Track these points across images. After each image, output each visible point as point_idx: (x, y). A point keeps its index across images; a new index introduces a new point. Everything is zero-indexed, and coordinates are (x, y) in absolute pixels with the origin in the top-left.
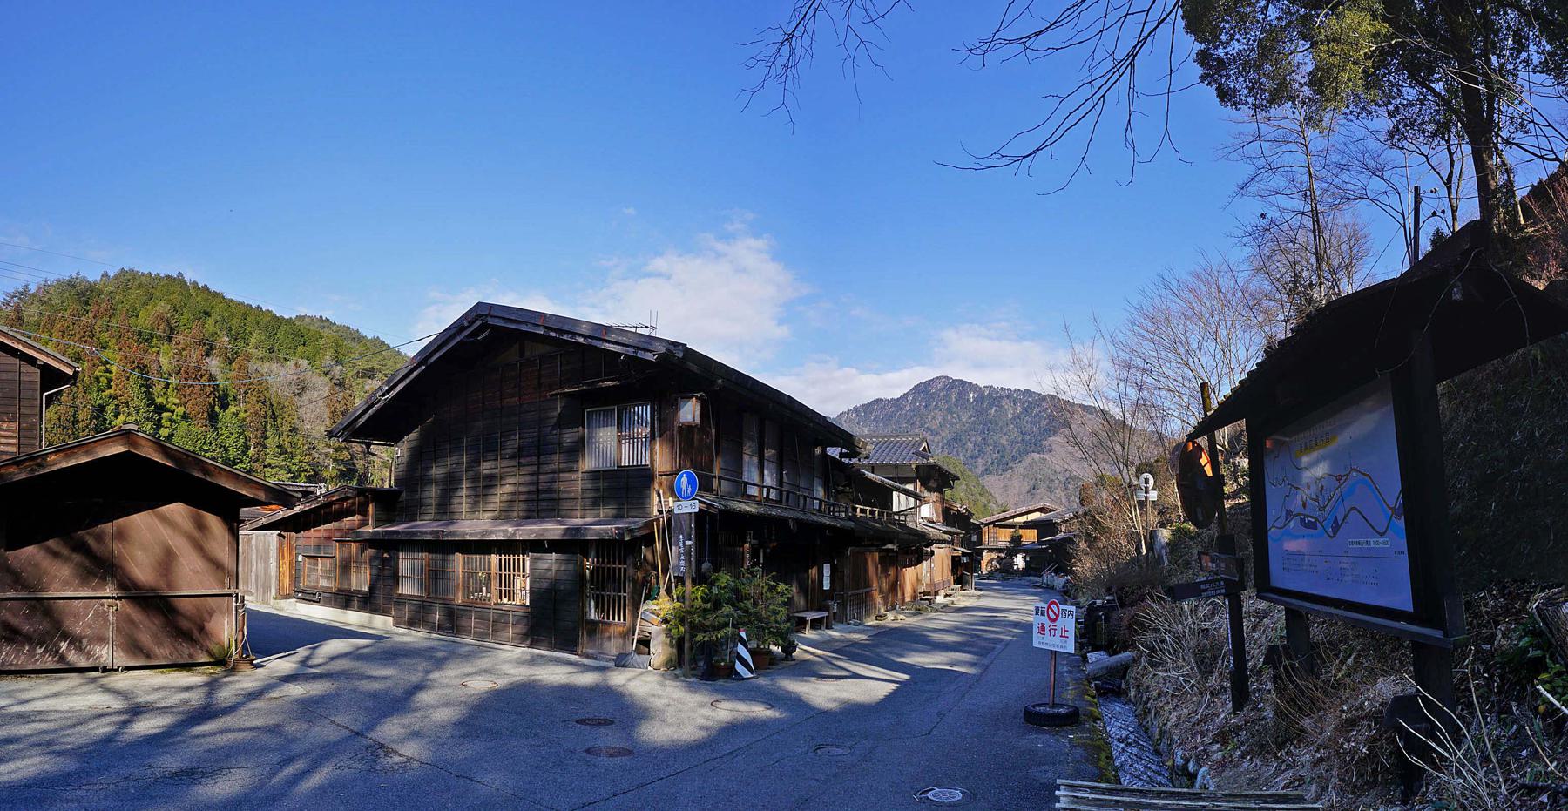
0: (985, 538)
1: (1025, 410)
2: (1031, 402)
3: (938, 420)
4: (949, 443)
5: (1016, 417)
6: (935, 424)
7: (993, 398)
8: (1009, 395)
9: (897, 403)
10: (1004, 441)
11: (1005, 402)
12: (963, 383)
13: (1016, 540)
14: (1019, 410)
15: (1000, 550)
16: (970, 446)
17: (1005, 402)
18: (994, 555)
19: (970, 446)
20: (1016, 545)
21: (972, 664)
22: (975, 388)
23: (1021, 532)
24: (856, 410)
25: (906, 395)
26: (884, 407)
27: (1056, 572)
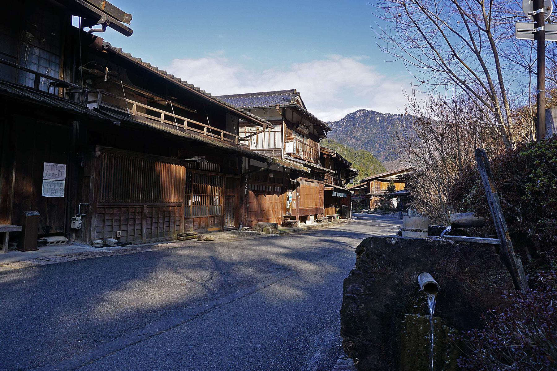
0: (372, 188)
4: (365, 144)
12: (373, 112)
13: (391, 189)
15: (381, 196)
16: (377, 145)
18: (378, 199)
19: (377, 145)
22: (380, 115)
23: (395, 184)
25: (343, 119)
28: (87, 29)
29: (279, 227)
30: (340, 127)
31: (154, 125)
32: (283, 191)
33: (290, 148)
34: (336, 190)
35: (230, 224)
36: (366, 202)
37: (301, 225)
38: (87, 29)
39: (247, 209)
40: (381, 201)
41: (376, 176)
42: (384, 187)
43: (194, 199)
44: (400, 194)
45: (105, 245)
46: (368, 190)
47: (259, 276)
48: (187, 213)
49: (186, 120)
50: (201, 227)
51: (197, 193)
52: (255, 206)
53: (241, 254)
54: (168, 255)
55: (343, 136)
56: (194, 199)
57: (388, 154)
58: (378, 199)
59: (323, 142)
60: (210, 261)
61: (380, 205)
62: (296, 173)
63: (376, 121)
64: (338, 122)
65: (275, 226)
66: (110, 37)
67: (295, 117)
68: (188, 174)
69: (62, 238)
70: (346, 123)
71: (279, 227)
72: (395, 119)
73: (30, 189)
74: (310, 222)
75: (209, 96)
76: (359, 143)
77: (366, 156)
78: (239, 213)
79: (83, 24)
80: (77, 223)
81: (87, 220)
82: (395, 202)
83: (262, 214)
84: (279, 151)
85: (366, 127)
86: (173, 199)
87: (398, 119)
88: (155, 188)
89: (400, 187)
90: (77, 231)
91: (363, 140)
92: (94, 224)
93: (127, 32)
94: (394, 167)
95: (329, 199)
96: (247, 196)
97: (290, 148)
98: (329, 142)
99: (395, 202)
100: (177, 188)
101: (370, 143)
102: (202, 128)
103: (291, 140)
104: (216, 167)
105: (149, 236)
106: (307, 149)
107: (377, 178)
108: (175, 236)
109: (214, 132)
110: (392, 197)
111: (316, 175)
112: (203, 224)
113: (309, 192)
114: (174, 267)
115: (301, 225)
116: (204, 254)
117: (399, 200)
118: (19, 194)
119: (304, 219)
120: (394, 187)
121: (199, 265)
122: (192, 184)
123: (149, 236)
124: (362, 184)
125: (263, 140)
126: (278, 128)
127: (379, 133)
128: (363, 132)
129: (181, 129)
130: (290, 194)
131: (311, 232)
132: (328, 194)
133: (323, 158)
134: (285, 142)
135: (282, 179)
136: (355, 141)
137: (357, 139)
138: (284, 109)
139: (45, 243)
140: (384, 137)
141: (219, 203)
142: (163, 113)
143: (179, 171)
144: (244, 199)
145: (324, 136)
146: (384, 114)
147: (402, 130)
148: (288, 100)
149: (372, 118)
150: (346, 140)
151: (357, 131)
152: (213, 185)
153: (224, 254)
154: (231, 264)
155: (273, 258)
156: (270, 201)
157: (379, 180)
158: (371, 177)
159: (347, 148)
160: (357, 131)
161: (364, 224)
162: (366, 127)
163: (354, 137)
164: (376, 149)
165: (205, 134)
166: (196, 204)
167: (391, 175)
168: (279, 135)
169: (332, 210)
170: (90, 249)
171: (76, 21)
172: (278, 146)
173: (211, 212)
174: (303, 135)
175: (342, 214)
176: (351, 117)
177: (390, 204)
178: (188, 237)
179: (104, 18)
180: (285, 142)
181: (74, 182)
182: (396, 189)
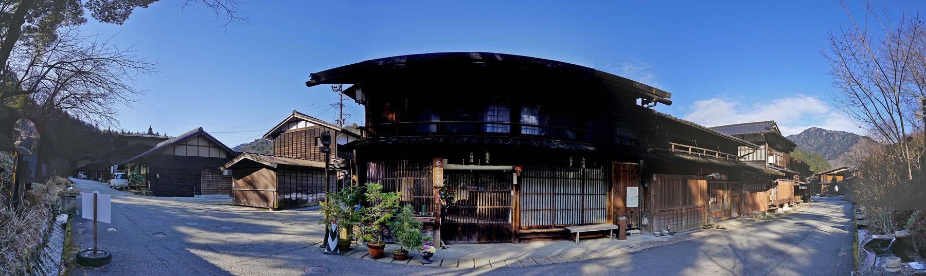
13: (834, 180)
22: (825, 131)
28: (645, 106)
29: (767, 214)
31: (685, 157)
32: (768, 189)
33: (771, 160)
34: (801, 185)
35: (735, 214)
36: (818, 190)
37: (780, 210)
38: (645, 106)
39: (745, 204)
42: (830, 178)
43: (712, 200)
45: (662, 235)
47: (765, 261)
48: (708, 209)
49: (705, 150)
50: (717, 218)
51: (714, 196)
52: (750, 201)
53: (749, 241)
54: (702, 244)
56: (712, 200)
59: (792, 154)
60: (730, 250)
62: (776, 177)
65: (764, 213)
66: (659, 108)
67: (770, 137)
68: (708, 185)
69: (637, 231)
71: (767, 214)
73: (620, 203)
74: (786, 208)
75: (704, 128)
78: (742, 208)
79: (643, 103)
80: (645, 221)
81: (651, 219)
82: (837, 188)
83: (755, 206)
84: (764, 162)
86: (700, 202)
88: (689, 198)
90: (645, 226)
92: (655, 222)
93: (669, 103)
94: (837, 165)
95: (797, 191)
96: (745, 195)
97: (771, 160)
99: (837, 188)
100: (702, 195)
101: (819, 148)
102: (715, 154)
103: (771, 155)
104: (725, 177)
105: (687, 227)
106: (781, 159)
108: (701, 226)
109: (722, 155)
111: (789, 176)
112: (718, 216)
113: (784, 188)
114: (710, 256)
115: (780, 210)
116: (725, 242)
118: (616, 207)
119: (781, 206)
121: (724, 255)
122: (711, 191)
123: (687, 227)
125: (750, 156)
126: (762, 147)
129: (702, 156)
130: (772, 190)
131: (789, 216)
132: (796, 188)
133: (792, 164)
134: (767, 156)
135: (767, 181)
138: (766, 135)
139: (629, 234)
141: (727, 202)
142: (691, 147)
143: (703, 183)
144: (743, 197)
145: (792, 150)
148: (769, 129)
152: (723, 189)
153: (741, 241)
154: (745, 252)
155: (769, 243)
156: (761, 197)
161: (820, 206)
165: (716, 159)
166: (714, 203)
168: (763, 151)
169: (798, 198)
170: (654, 238)
171: (639, 102)
172: (763, 159)
173: (723, 207)
174: (779, 150)
175: (805, 200)
178: (710, 226)
179: (656, 98)
180: (767, 156)
181: (645, 195)
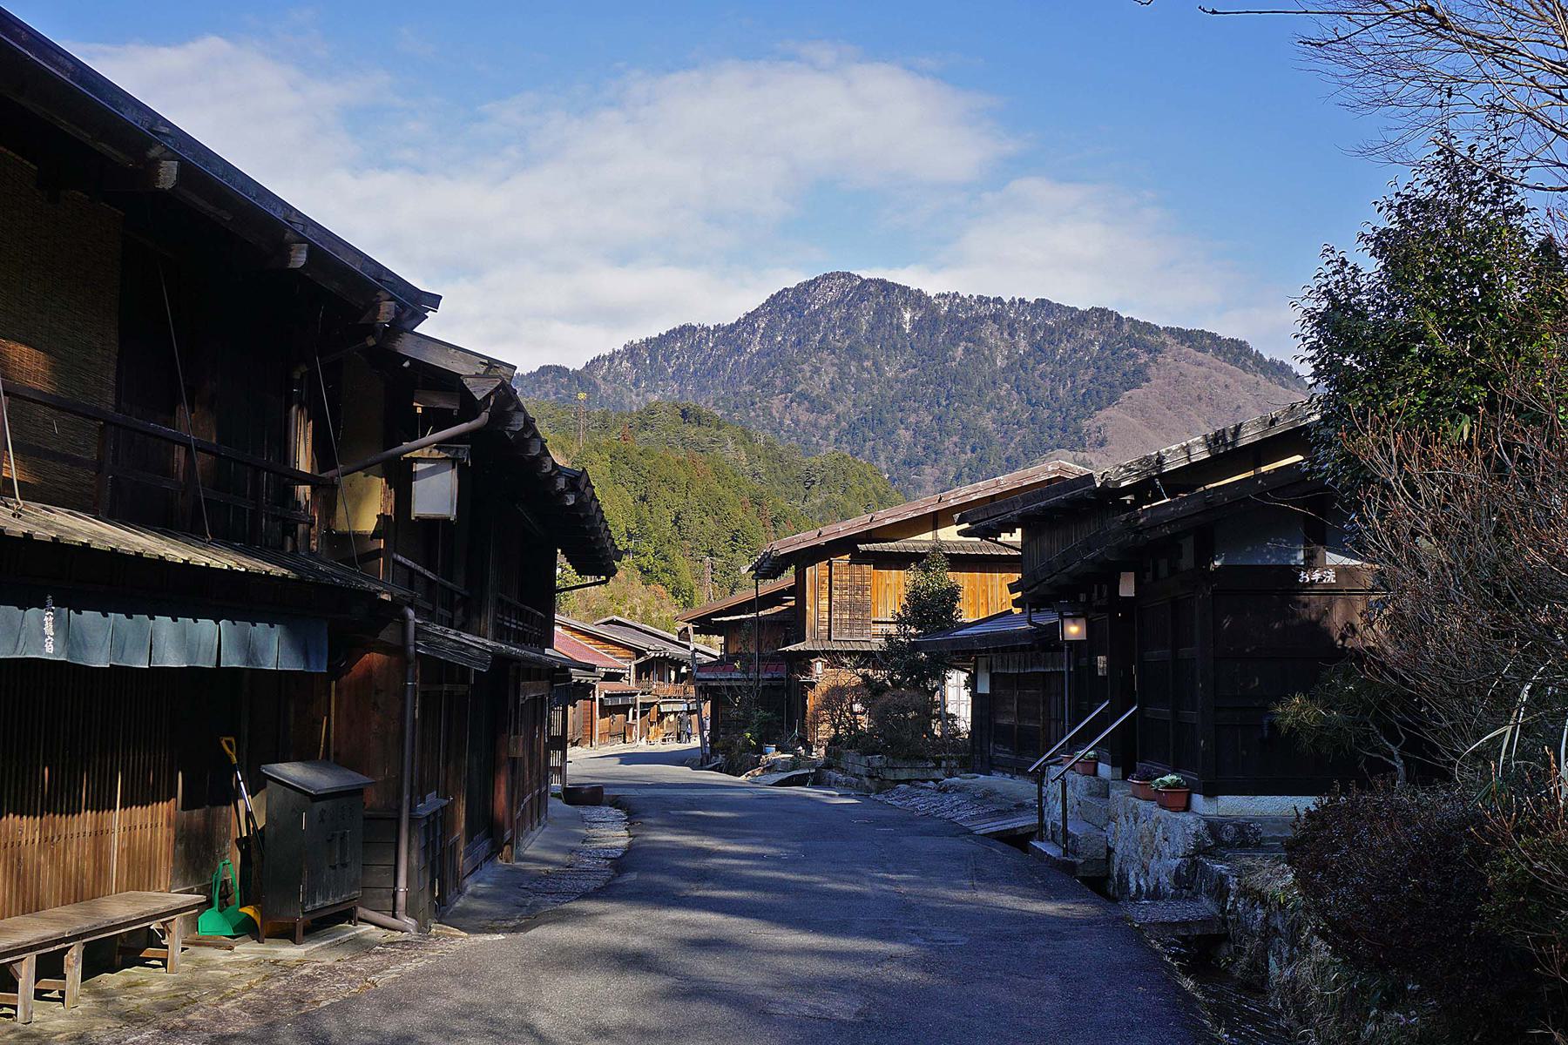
0: (817, 609)
1: (1037, 347)
2: (1050, 324)
3: (829, 374)
4: (853, 429)
5: (1017, 365)
6: (819, 386)
7: (963, 320)
8: (999, 313)
9: (730, 336)
10: (987, 422)
11: (988, 331)
12: (886, 287)
13: (930, 610)
14: (1023, 347)
15: (866, 658)
16: (904, 435)
17: (988, 331)
18: (848, 677)
19: (904, 435)
20: (933, 636)
21: (907, 962)
22: (916, 299)
23: (963, 579)
24: (632, 352)
25: (752, 316)
26: (697, 347)
27: (1129, 755)
30: (739, 350)
40: (871, 690)
41: (842, 529)
44: (984, 638)
46: (794, 624)
55: (751, 394)
57: (952, 471)
58: (848, 677)
61: (864, 723)
63: (899, 327)
64: (732, 327)
70: (768, 336)
72: (979, 320)
76: (823, 423)
77: (853, 481)
82: (957, 696)
85: (854, 352)
87: (995, 318)
89: (986, 599)
91: (840, 409)
98: (684, 414)
101: (874, 423)
107: (845, 545)
110: (938, 668)
117: (984, 688)
120: (953, 593)
124: (768, 587)
127: (912, 381)
128: (842, 374)
136: (805, 417)
137: (818, 406)
140: (936, 395)
146: (932, 293)
147: (1009, 369)
149: (879, 312)
150: (767, 411)
151: (816, 371)
157: (860, 559)
158: (807, 538)
159: (770, 446)
160: (816, 371)
162: (854, 352)
163: (803, 396)
164: (901, 455)
167: (935, 520)
176: (784, 305)
177: (932, 709)
182: (967, 613)
